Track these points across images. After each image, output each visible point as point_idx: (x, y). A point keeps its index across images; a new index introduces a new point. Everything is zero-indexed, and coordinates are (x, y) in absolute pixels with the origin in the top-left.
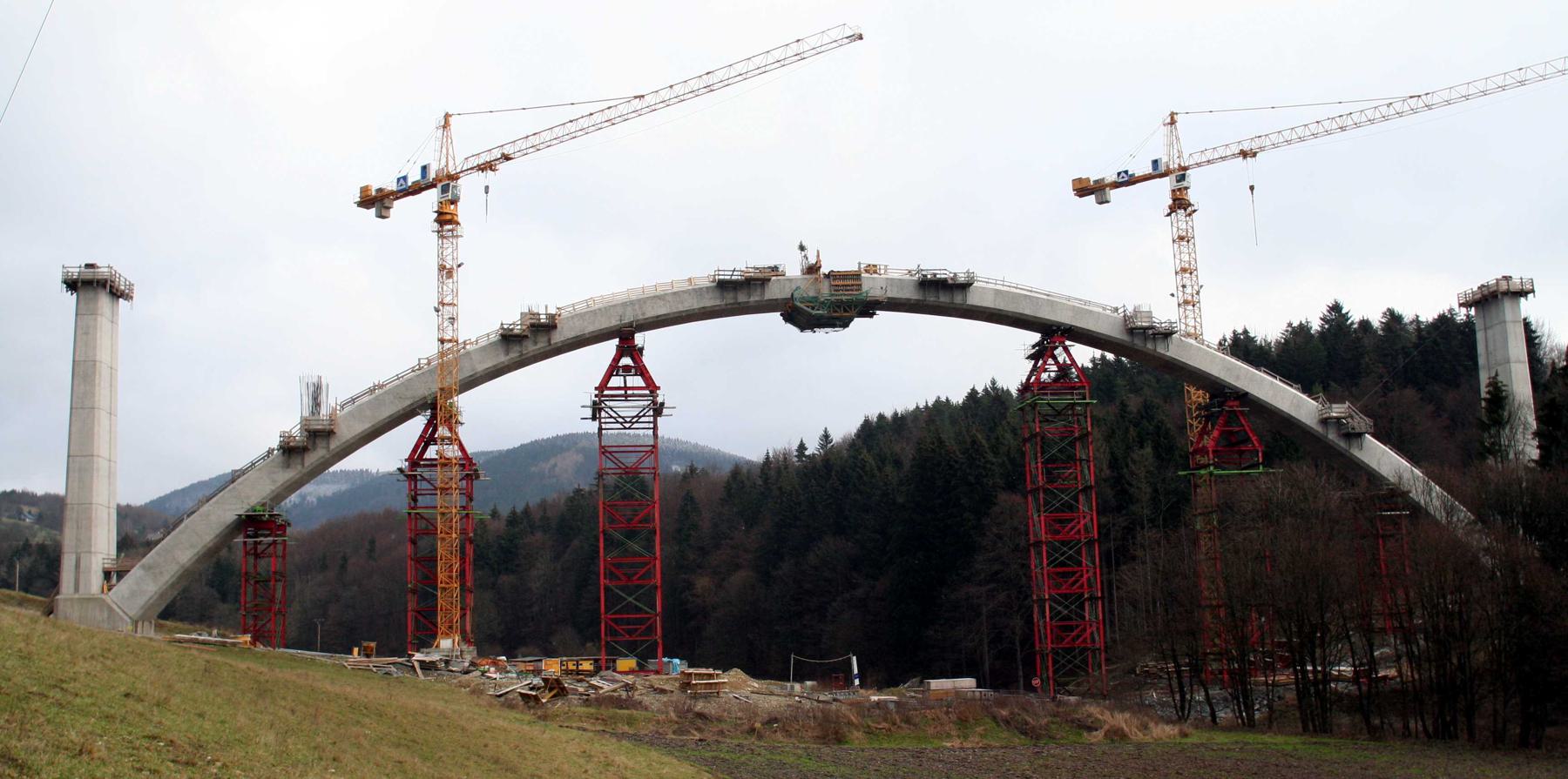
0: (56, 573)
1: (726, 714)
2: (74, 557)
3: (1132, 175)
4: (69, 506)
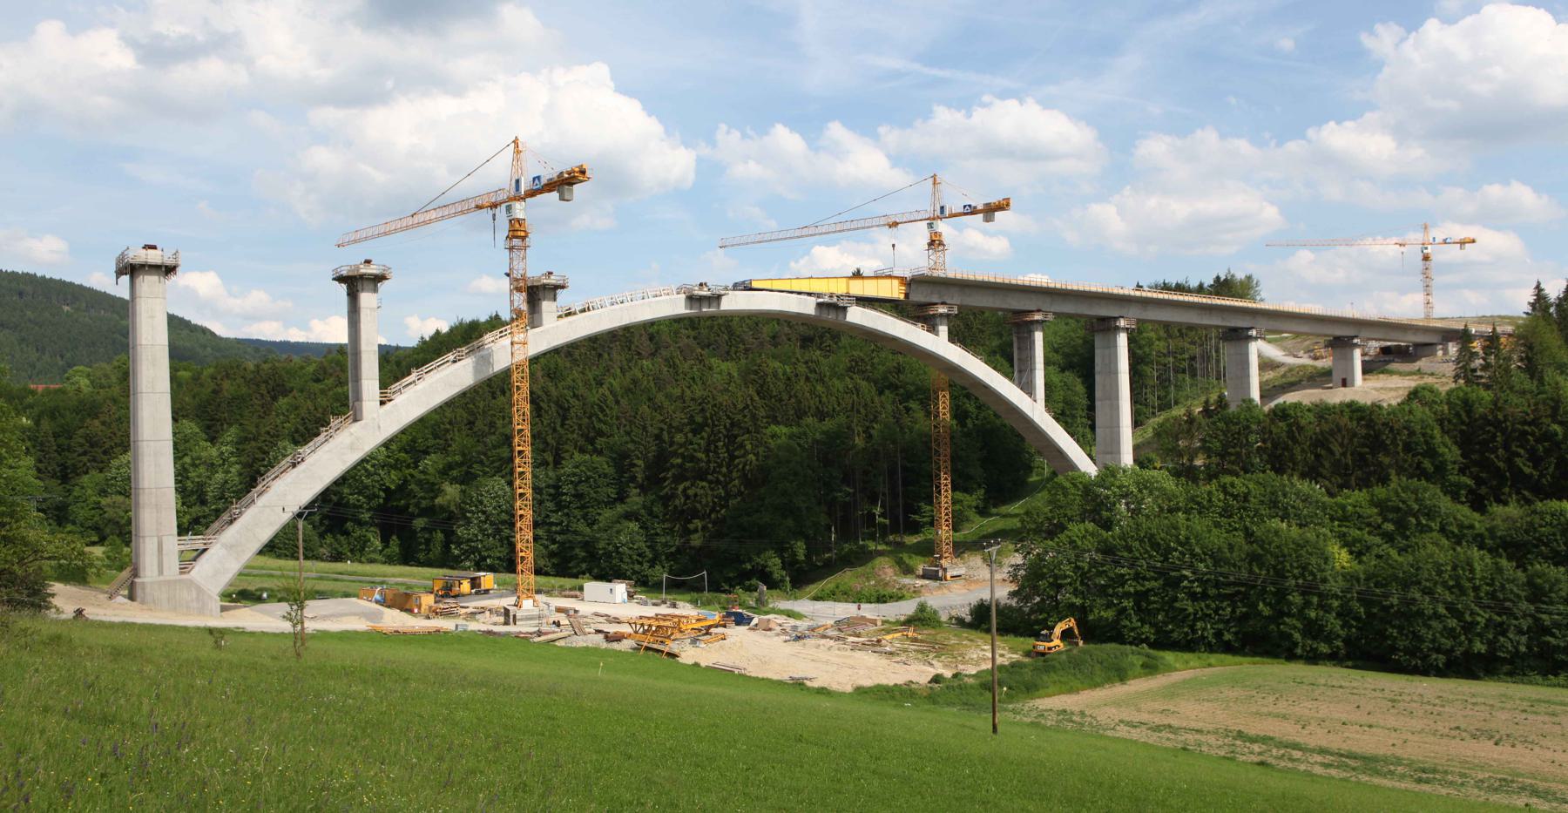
0: (1050, 355)
1: (1392, 416)
2: (155, 540)
3: (975, 207)
4: (146, 491)
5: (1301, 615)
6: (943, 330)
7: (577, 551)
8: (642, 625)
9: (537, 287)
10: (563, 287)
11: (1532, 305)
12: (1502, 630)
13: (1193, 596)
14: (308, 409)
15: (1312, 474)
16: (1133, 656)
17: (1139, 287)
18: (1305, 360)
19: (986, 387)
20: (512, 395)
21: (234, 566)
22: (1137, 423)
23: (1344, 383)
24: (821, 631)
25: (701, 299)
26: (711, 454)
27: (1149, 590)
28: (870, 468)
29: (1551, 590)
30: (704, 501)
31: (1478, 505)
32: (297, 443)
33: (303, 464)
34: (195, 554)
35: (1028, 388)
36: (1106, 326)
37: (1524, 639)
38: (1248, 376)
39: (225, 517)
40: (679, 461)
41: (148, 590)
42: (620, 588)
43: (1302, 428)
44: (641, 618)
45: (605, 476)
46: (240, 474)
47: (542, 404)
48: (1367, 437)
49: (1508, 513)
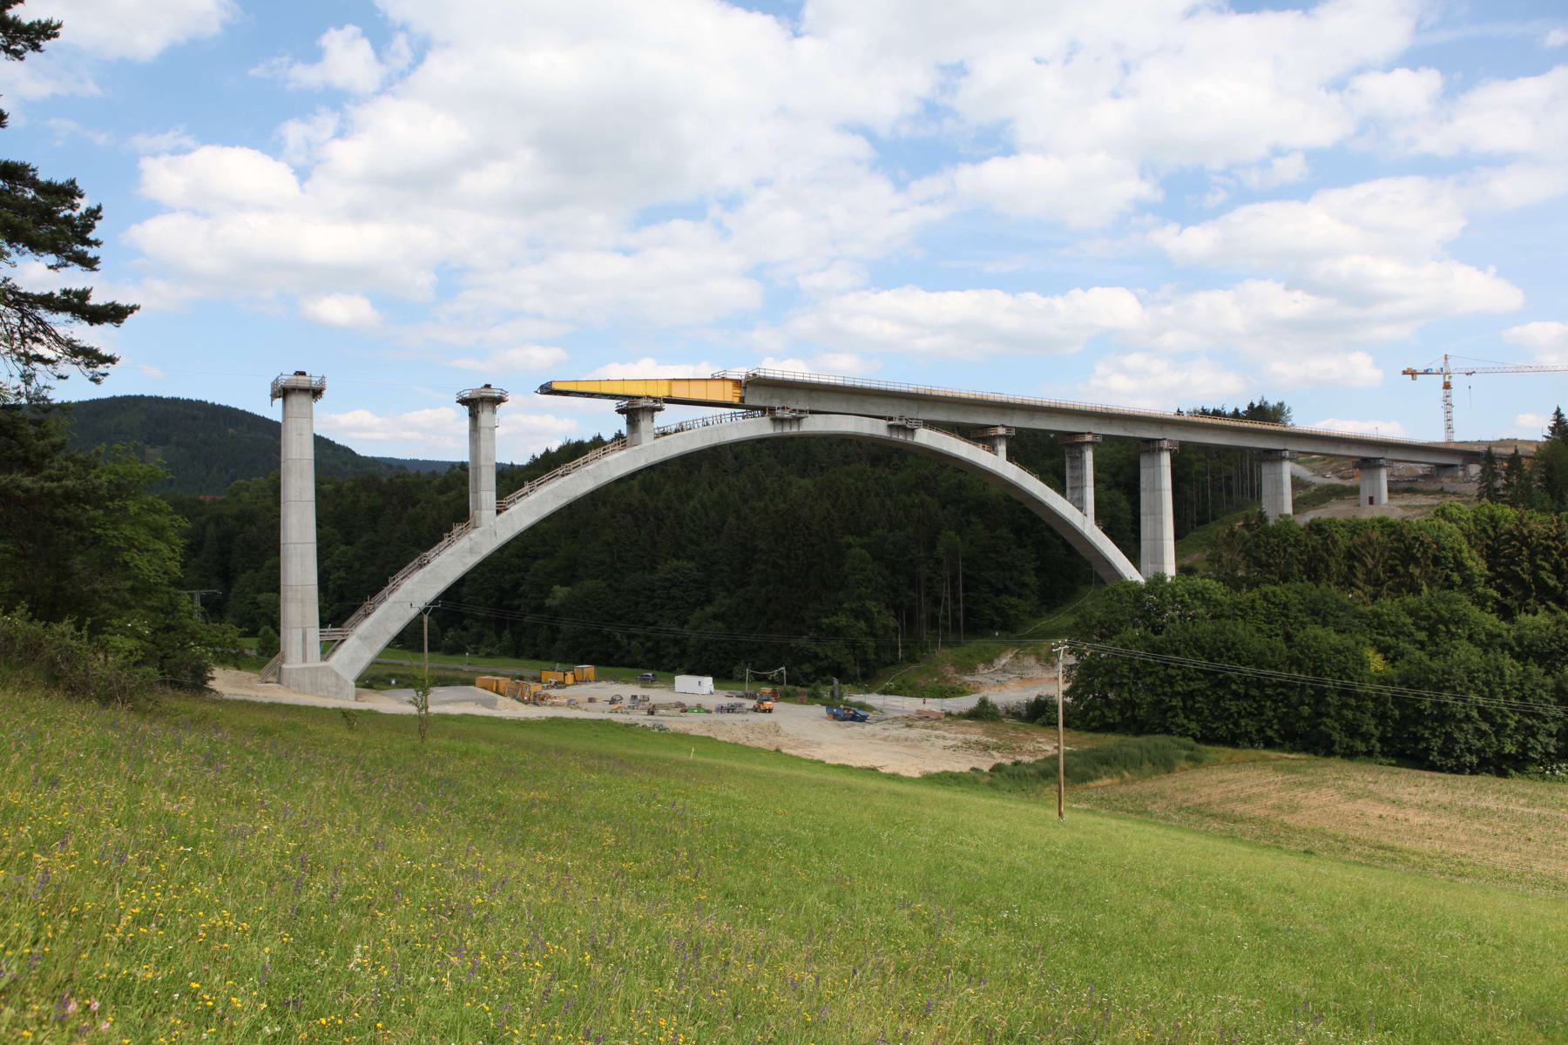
2: (300, 631)
6: (1002, 448)
17: (1179, 412)
31: (1506, 613)
35: (1079, 504)
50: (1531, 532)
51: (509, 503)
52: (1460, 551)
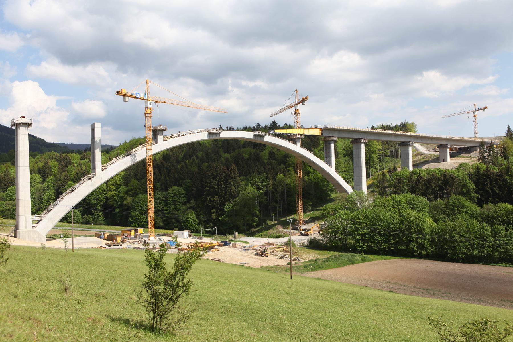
2: (24, 217)
5: (416, 242)
6: (299, 144)
7: (173, 220)
8: (191, 245)
9: (156, 130)
10: (165, 130)
11: (507, 134)
12: (483, 246)
13: (380, 235)
14: (79, 170)
15: (424, 194)
16: (358, 257)
17: (373, 127)
18: (432, 153)
19: (314, 163)
20: (147, 167)
21: (51, 225)
22: (368, 175)
23: (444, 161)
24: (254, 248)
25: (213, 134)
26: (219, 186)
27: (365, 233)
28: (275, 191)
29: (500, 233)
30: (217, 203)
31: (480, 204)
32: (74, 182)
33: (75, 191)
34: (38, 221)
35: (329, 163)
36: (357, 142)
37: (490, 249)
38: (408, 158)
39: (48, 209)
40: (208, 188)
41: (21, 234)
42: (186, 233)
43: (422, 177)
44: (191, 243)
45: (183, 194)
46: (54, 193)
47: (161, 168)
48: (443, 180)
49: (489, 207)
50: (490, 174)
51: (107, 166)
52: (466, 180)
